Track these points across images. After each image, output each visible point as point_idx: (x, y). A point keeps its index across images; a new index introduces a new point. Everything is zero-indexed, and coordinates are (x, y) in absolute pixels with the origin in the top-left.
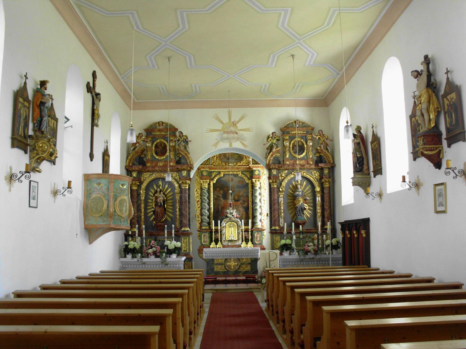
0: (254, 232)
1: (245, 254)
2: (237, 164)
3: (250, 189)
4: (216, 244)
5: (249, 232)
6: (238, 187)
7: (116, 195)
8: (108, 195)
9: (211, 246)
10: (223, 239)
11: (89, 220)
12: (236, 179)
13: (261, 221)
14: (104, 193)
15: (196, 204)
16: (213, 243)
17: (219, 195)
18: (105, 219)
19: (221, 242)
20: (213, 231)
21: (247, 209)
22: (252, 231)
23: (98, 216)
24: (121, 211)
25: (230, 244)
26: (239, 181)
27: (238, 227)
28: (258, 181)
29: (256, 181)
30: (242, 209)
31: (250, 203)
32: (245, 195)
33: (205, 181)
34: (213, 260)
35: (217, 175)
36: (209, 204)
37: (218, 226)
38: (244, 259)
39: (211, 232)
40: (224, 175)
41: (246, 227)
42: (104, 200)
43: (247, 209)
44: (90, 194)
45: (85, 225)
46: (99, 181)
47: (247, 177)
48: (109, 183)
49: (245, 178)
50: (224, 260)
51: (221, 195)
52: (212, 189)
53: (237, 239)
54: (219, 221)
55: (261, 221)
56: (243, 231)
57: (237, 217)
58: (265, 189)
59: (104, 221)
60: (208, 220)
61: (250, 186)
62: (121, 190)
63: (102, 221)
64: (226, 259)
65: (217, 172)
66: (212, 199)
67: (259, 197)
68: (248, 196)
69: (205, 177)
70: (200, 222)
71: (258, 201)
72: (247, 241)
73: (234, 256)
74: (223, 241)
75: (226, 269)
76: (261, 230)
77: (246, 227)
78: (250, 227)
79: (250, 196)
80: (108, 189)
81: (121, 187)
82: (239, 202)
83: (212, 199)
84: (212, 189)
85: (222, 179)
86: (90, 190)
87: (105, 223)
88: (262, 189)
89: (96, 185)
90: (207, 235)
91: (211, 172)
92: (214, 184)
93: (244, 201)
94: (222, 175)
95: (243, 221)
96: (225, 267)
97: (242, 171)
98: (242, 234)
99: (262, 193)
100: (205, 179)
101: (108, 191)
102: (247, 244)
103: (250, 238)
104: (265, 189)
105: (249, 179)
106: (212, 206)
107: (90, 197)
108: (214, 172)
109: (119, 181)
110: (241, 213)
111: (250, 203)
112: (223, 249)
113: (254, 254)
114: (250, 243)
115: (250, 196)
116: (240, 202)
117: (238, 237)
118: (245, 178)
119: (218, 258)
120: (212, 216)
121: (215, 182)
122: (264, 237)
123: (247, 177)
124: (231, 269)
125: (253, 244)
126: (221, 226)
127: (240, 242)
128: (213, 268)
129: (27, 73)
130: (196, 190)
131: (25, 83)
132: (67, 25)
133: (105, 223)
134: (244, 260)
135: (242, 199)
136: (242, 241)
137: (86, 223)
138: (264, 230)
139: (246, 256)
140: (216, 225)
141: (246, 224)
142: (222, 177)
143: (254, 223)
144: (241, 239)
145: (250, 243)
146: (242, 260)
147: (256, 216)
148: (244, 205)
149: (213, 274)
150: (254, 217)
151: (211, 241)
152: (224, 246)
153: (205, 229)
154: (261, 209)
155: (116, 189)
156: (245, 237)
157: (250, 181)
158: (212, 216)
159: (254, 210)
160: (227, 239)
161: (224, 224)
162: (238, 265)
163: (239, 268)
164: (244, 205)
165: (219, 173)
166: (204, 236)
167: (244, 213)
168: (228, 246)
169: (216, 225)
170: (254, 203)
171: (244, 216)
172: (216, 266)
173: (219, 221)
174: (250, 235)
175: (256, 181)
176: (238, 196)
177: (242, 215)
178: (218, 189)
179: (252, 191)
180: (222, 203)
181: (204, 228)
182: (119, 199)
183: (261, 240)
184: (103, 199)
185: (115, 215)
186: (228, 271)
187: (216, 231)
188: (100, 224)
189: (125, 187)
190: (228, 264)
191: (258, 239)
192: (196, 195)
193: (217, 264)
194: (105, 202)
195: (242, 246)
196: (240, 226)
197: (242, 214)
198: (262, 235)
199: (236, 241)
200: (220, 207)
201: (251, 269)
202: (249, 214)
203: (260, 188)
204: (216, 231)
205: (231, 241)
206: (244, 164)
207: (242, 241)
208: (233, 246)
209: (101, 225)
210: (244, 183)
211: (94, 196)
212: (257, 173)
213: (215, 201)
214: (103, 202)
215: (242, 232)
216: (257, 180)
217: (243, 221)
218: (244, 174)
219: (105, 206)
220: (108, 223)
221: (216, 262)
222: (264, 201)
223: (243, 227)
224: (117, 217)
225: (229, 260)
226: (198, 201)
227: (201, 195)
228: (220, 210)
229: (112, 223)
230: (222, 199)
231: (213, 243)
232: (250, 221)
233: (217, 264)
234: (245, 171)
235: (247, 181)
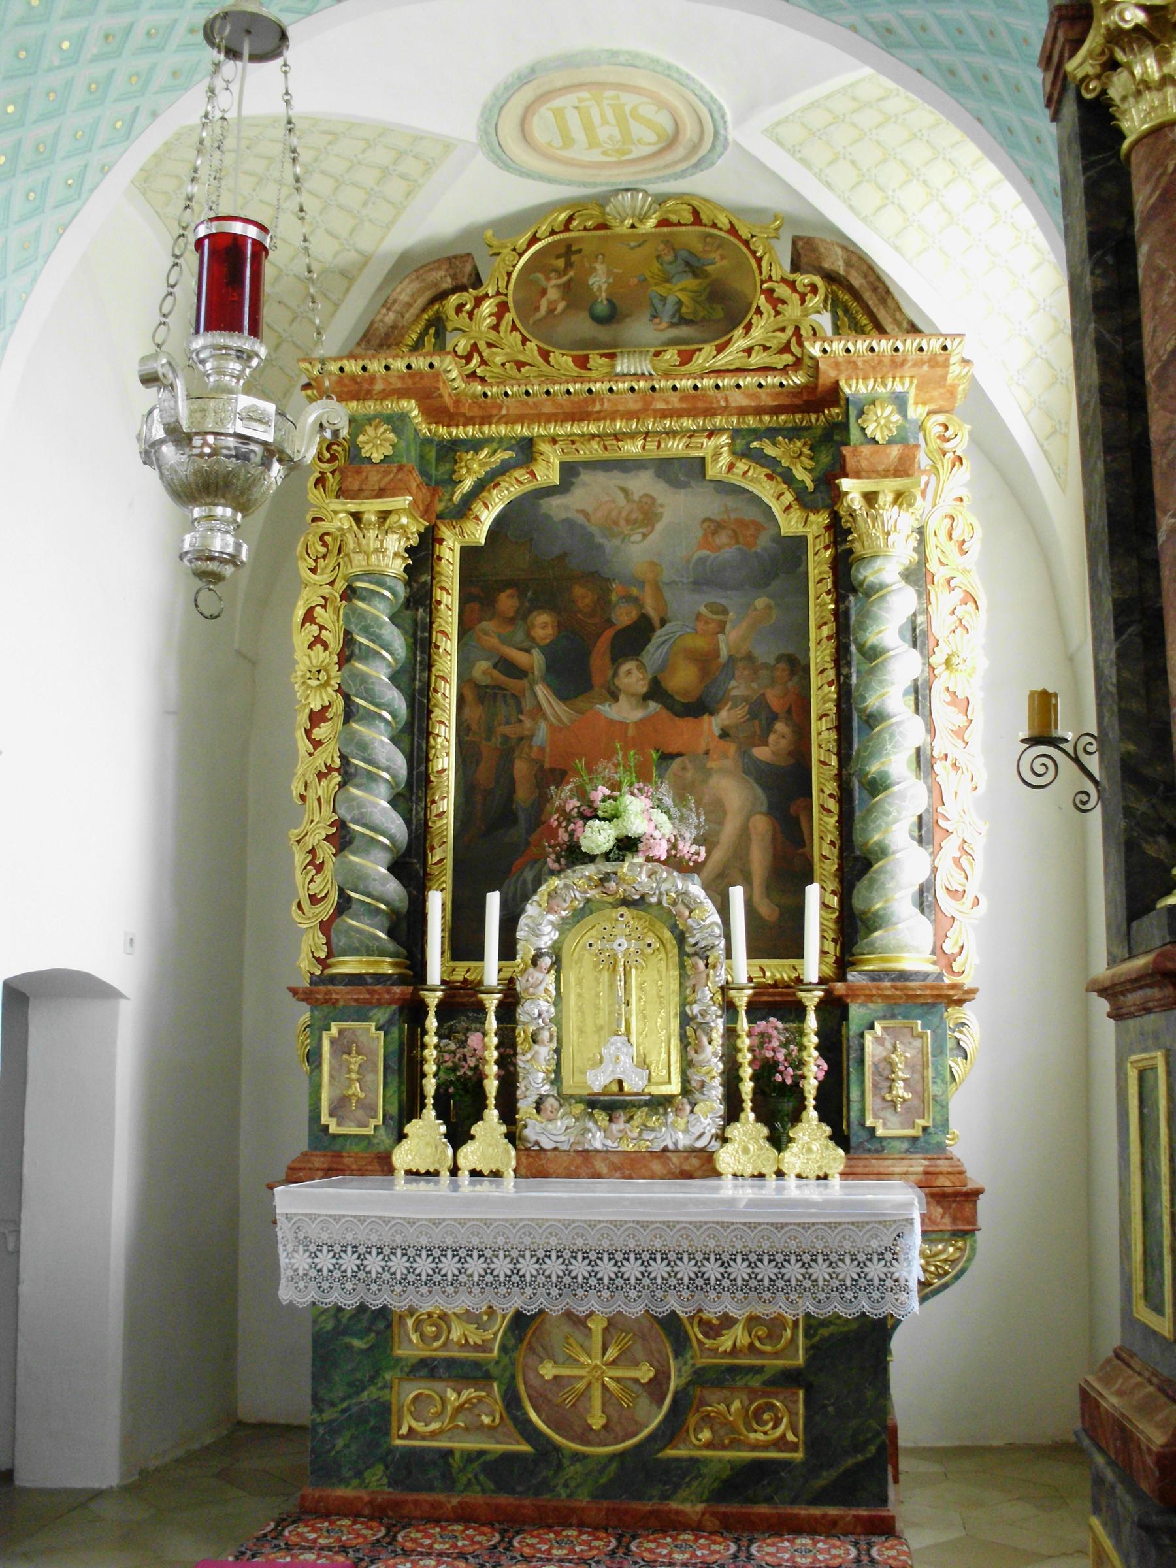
0: (856, 1012)
1: (740, 1270)
2: (686, 358)
3: (820, 601)
4: (458, 1136)
5: (799, 1011)
6: (705, 579)
9: (403, 1157)
10: (534, 1080)
12: (681, 508)
13: (925, 898)
15: (304, 745)
16: (427, 1129)
17: (520, 658)
19: (508, 1112)
20: (433, 999)
21: (786, 789)
22: (834, 1010)
25: (597, 1140)
26: (714, 527)
27: (687, 951)
28: (899, 497)
29: (870, 498)
30: (736, 794)
31: (822, 733)
32: (766, 653)
33: (371, 508)
34: (379, 1323)
35: (504, 469)
36: (415, 734)
37: (478, 954)
38: (727, 1321)
39: (414, 1012)
40: (569, 471)
41: (777, 970)
43: (786, 789)
47: (788, 478)
49: (767, 491)
50: (500, 1326)
51: (536, 660)
52: (449, 602)
53: (675, 1088)
54: (493, 901)
55: (925, 898)
56: (742, 999)
57: (675, 862)
58: (970, 598)
60: (393, 888)
61: (818, 564)
64: (520, 1322)
65: (502, 443)
66: (447, 695)
67: (902, 666)
68: (798, 667)
69: (374, 479)
70: (326, 910)
71: (890, 694)
72: (777, 1107)
73: (617, 1284)
74: (525, 1107)
75: (527, 1431)
76: (929, 1000)
77: (777, 970)
78: (812, 966)
79: (820, 655)
82: (713, 724)
83: (447, 695)
84: (449, 602)
85: (555, 506)
88: (942, 600)
90: (372, 1036)
91: (450, 450)
92: (469, 554)
93: (762, 717)
94: (548, 472)
95: (737, 895)
96: (512, 1401)
97: (736, 433)
98: (731, 1034)
99: (940, 625)
100: (381, 493)
102: (778, 1141)
103: (811, 1087)
104: (970, 598)
105: (804, 501)
106: (445, 762)
108: (475, 445)
110: (730, 829)
111: (822, 733)
112: (514, 1202)
113: (848, 1270)
114: (810, 1131)
115: (820, 655)
116: (725, 717)
117: (687, 1064)
118: (767, 491)
119: (430, 1304)
120: (442, 855)
121: (479, 533)
122: (958, 1066)
123: (788, 478)
124: (585, 1435)
125: (840, 1138)
126: (508, 950)
127: (708, 1114)
128: (384, 1411)
130: (309, 617)
134: (737, 1336)
135: (738, 688)
136: (732, 1113)
138: (957, 998)
139: (753, 1287)
140: (465, 942)
141: (777, 936)
142: (548, 491)
143: (852, 928)
144: (716, 1091)
145: (810, 1131)
146: (713, 1329)
147: (883, 851)
148: (762, 753)
149: (376, 1477)
150: (857, 864)
151: (411, 1108)
152: (535, 1164)
153: (355, 980)
154: (936, 794)
156: (765, 1071)
157: (823, 518)
158: (442, 855)
159: (858, 792)
160: (570, 1085)
161: (540, 926)
162: (656, 1388)
163: (673, 1428)
164: (762, 753)
165: (526, 450)
166: (342, 1047)
167: (761, 825)
168: (583, 1163)
169: (465, 942)
170: (854, 723)
171: (759, 859)
172: (411, 1391)
173: (493, 901)
174: (806, 1063)
175: (870, 498)
176: (705, 661)
177: (740, 852)
178: (507, 602)
179: (841, 618)
180: (542, 733)
181: (349, 965)
183: (930, 1104)
186: (546, 1452)
187: (461, 1004)
190: (548, 1371)
191: (900, 1089)
192: (305, 659)
193: (427, 1369)
195: (727, 1159)
196: (703, 953)
197: (744, 834)
198: (946, 1046)
199: (660, 1104)
200: (521, 768)
201: (816, 1442)
202: (809, 826)
203: (917, 576)
204: (461, 1004)
205: (611, 1104)
206: (757, 360)
207: (732, 1113)
208: (630, 1166)
210: (764, 542)
212: (879, 423)
213: (475, 713)
215: (729, 1008)
216: (887, 488)
217: (737, 895)
218: (759, 458)
221: (411, 1346)
222: (965, 706)
223: (742, 968)
225: (557, 1333)
226: (317, 718)
227: (347, 655)
228: (523, 795)
230: (541, 691)
231: (427, 1129)
232: (815, 900)
233: (427, 1369)
234: (771, 434)
235: (791, 524)
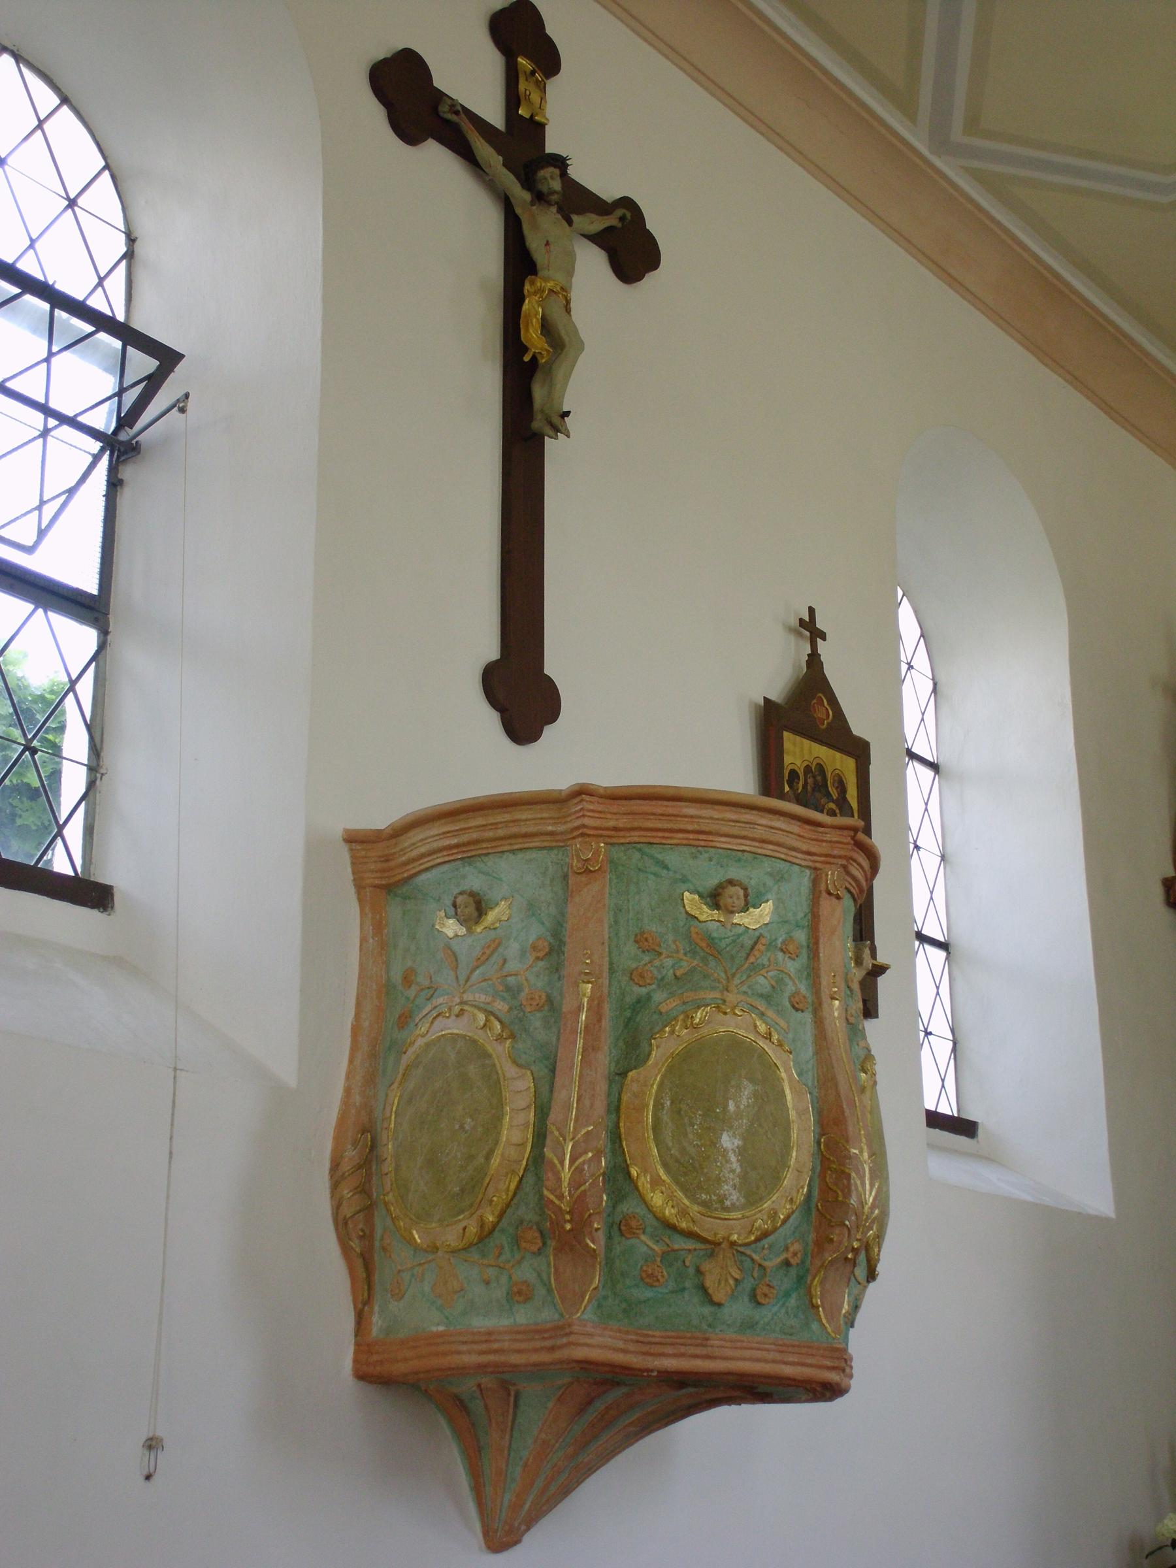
7: (641, 1003)
8: (551, 1005)
11: (398, 1294)
14: (512, 992)
18: (526, 1272)
23: (451, 1237)
24: (691, 1172)
42: (510, 1070)
44: (405, 1020)
45: (364, 1346)
46: (474, 880)
48: (572, 879)
59: (520, 1294)
62: (707, 947)
63: (499, 1293)
80: (554, 951)
81: (705, 913)
86: (408, 978)
87: (523, 1316)
89: (451, 928)
101: (557, 969)
107: (399, 1048)
109: (673, 858)
129: (812, 611)
131: (814, 660)
132: (798, 169)
133: (523, 1316)
137: (377, 1324)
155: (643, 941)
182: (664, 1048)
184: (500, 1051)
185: (621, 1228)
188: (480, 1323)
189: (759, 917)
194: (520, 1089)
209: (489, 1335)
211: (439, 1027)
214: (494, 1083)
219: (515, 1131)
220: (547, 1316)
224: (646, 1244)
229: (585, 1314)
